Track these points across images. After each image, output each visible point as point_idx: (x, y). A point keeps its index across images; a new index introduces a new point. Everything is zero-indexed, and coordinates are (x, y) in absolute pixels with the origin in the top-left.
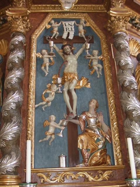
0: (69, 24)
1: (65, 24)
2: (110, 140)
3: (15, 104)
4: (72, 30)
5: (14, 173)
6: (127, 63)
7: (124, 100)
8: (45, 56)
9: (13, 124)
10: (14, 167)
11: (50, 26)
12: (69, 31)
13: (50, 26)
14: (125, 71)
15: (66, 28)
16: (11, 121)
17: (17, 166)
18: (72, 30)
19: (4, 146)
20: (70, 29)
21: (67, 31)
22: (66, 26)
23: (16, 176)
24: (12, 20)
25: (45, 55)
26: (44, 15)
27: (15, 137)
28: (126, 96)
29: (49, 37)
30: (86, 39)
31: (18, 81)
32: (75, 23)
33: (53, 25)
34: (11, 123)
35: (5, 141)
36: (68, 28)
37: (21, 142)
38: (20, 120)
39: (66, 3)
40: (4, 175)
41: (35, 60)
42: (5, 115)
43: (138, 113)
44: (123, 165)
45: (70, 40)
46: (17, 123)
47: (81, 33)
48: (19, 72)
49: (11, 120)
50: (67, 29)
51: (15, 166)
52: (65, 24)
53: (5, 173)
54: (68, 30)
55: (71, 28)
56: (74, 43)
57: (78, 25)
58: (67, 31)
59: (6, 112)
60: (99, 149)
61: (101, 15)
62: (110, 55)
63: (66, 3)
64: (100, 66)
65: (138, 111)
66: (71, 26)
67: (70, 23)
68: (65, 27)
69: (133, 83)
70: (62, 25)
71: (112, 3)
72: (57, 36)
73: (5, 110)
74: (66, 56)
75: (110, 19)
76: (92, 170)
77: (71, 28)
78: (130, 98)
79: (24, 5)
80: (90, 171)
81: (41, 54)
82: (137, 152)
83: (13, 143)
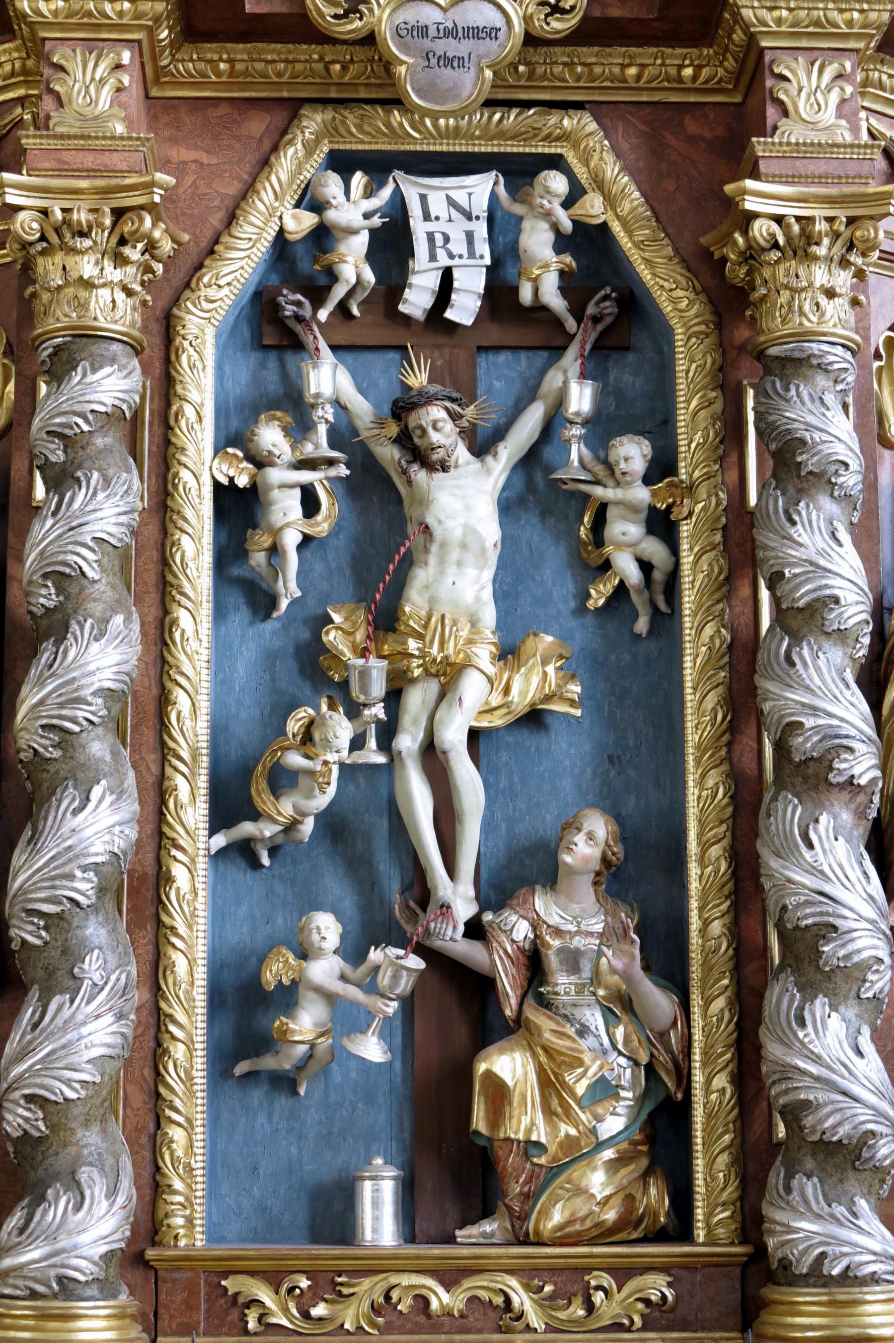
0: (451, 202)
1: (423, 198)
2: (679, 1084)
3: (92, 874)
4: (472, 254)
5: (101, 1290)
6: (828, 592)
7: (778, 855)
8: (275, 475)
9: (88, 1002)
10: (101, 1257)
11: (309, 220)
12: (448, 262)
13: (309, 220)
14: (806, 652)
15: (431, 237)
16: (74, 986)
17: (112, 1251)
18: (472, 254)
19: (36, 1134)
20: (458, 246)
21: (433, 257)
22: (427, 217)
23: (112, 1303)
24: (43, 238)
25: (272, 464)
26: (267, 118)
27: (98, 1079)
28: (792, 831)
29: (307, 311)
30: (571, 324)
31: (104, 712)
32: (501, 190)
33: (332, 215)
34: (72, 1001)
35: (42, 1108)
36: (447, 239)
37: (128, 1087)
38: (124, 976)
39: (434, 61)
40: (42, 1297)
41: (207, 507)
42: (29, 938)
43: (850, 947)
44: (741, 1243)
45: (453, 326)
46: (110, 997)
47: (536, 281)
48: (109, 650)
49: (74, 977)
50: (439, 240)
51: (103, 1249)
52: (423, 198)
53: (50, 1287)
54: (441, 254)
55: (470, 236)
56: (481, 349)
57: (518, 209)
58: (433, 257)
59: (42, 923)
60: (600, 1146)
61: (692, 127)
62: (733, 476)
63: (434, 61)
64: (655, 550)
65: (852, 940)
66: (469, 217)
67: (460, 197)
68: (419, 228)
69: (845, 742)
70: (399, 206)
71: (769, 83)
72: (361, 296)
73: (31, 912)
74: (420, 475)
75: (745, 232)
76: (553, 1270)
77: (470, 236)
78: (810, 846)
79: (123, 96)
80: (536, 1271)
81: (250, 458)
82: (814, 1185)
83: (88, 1114)
